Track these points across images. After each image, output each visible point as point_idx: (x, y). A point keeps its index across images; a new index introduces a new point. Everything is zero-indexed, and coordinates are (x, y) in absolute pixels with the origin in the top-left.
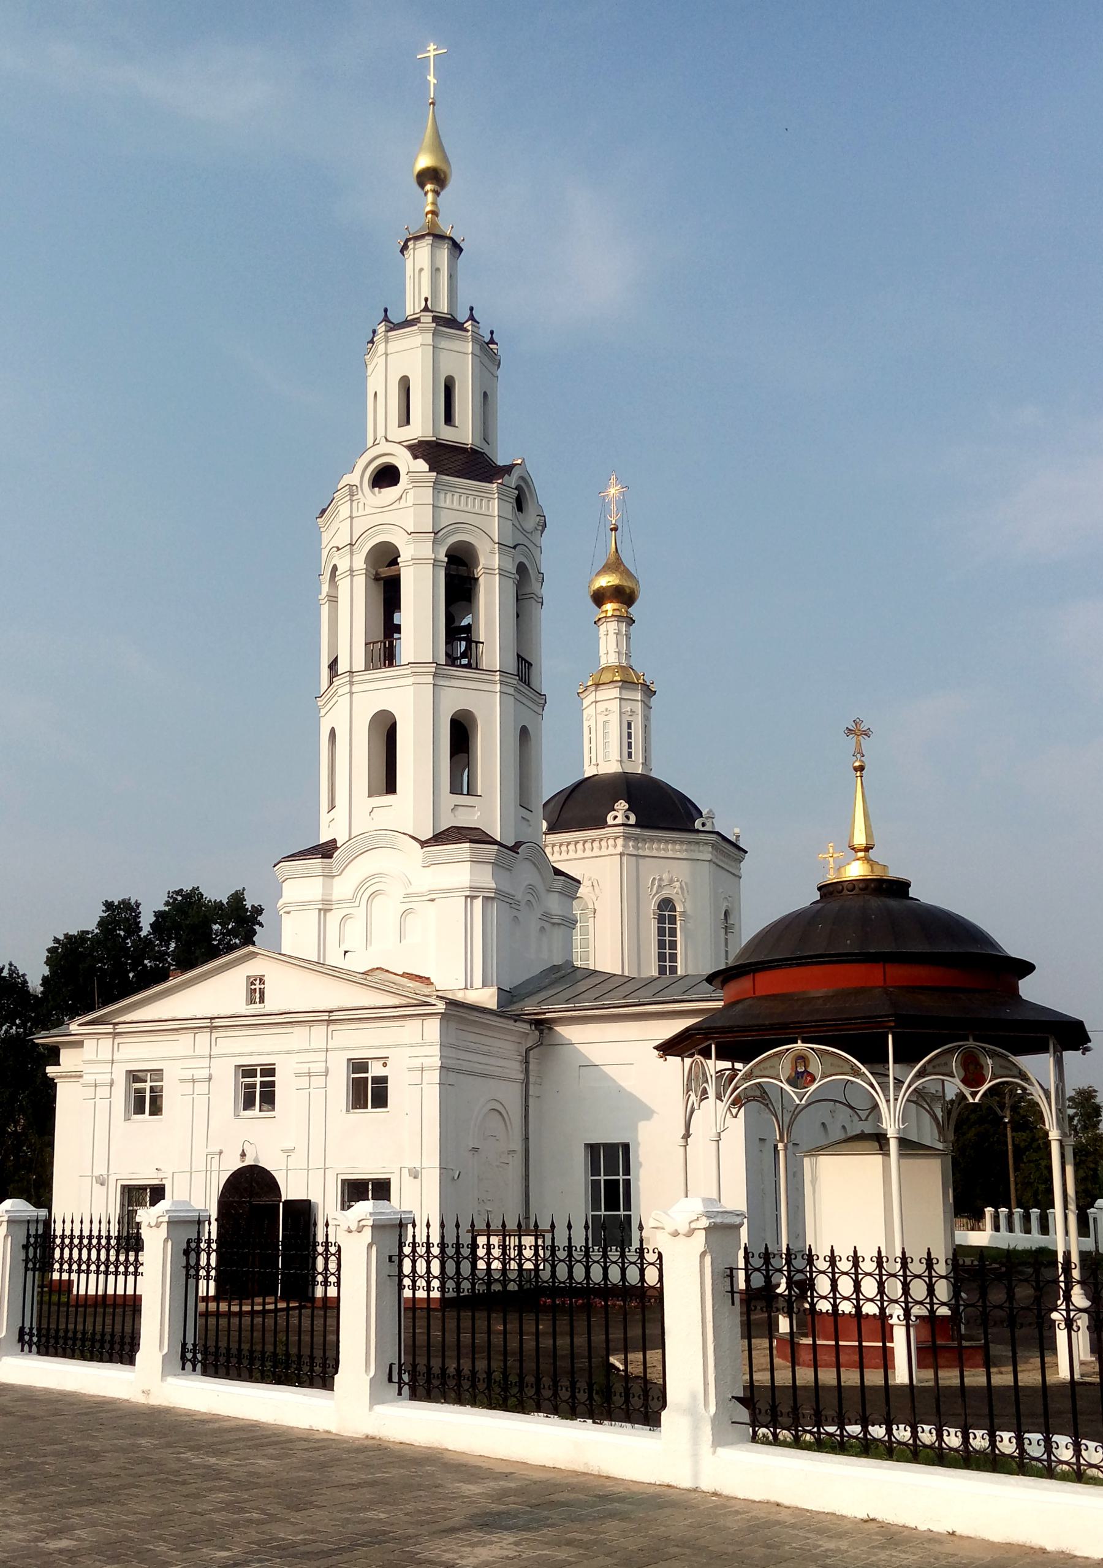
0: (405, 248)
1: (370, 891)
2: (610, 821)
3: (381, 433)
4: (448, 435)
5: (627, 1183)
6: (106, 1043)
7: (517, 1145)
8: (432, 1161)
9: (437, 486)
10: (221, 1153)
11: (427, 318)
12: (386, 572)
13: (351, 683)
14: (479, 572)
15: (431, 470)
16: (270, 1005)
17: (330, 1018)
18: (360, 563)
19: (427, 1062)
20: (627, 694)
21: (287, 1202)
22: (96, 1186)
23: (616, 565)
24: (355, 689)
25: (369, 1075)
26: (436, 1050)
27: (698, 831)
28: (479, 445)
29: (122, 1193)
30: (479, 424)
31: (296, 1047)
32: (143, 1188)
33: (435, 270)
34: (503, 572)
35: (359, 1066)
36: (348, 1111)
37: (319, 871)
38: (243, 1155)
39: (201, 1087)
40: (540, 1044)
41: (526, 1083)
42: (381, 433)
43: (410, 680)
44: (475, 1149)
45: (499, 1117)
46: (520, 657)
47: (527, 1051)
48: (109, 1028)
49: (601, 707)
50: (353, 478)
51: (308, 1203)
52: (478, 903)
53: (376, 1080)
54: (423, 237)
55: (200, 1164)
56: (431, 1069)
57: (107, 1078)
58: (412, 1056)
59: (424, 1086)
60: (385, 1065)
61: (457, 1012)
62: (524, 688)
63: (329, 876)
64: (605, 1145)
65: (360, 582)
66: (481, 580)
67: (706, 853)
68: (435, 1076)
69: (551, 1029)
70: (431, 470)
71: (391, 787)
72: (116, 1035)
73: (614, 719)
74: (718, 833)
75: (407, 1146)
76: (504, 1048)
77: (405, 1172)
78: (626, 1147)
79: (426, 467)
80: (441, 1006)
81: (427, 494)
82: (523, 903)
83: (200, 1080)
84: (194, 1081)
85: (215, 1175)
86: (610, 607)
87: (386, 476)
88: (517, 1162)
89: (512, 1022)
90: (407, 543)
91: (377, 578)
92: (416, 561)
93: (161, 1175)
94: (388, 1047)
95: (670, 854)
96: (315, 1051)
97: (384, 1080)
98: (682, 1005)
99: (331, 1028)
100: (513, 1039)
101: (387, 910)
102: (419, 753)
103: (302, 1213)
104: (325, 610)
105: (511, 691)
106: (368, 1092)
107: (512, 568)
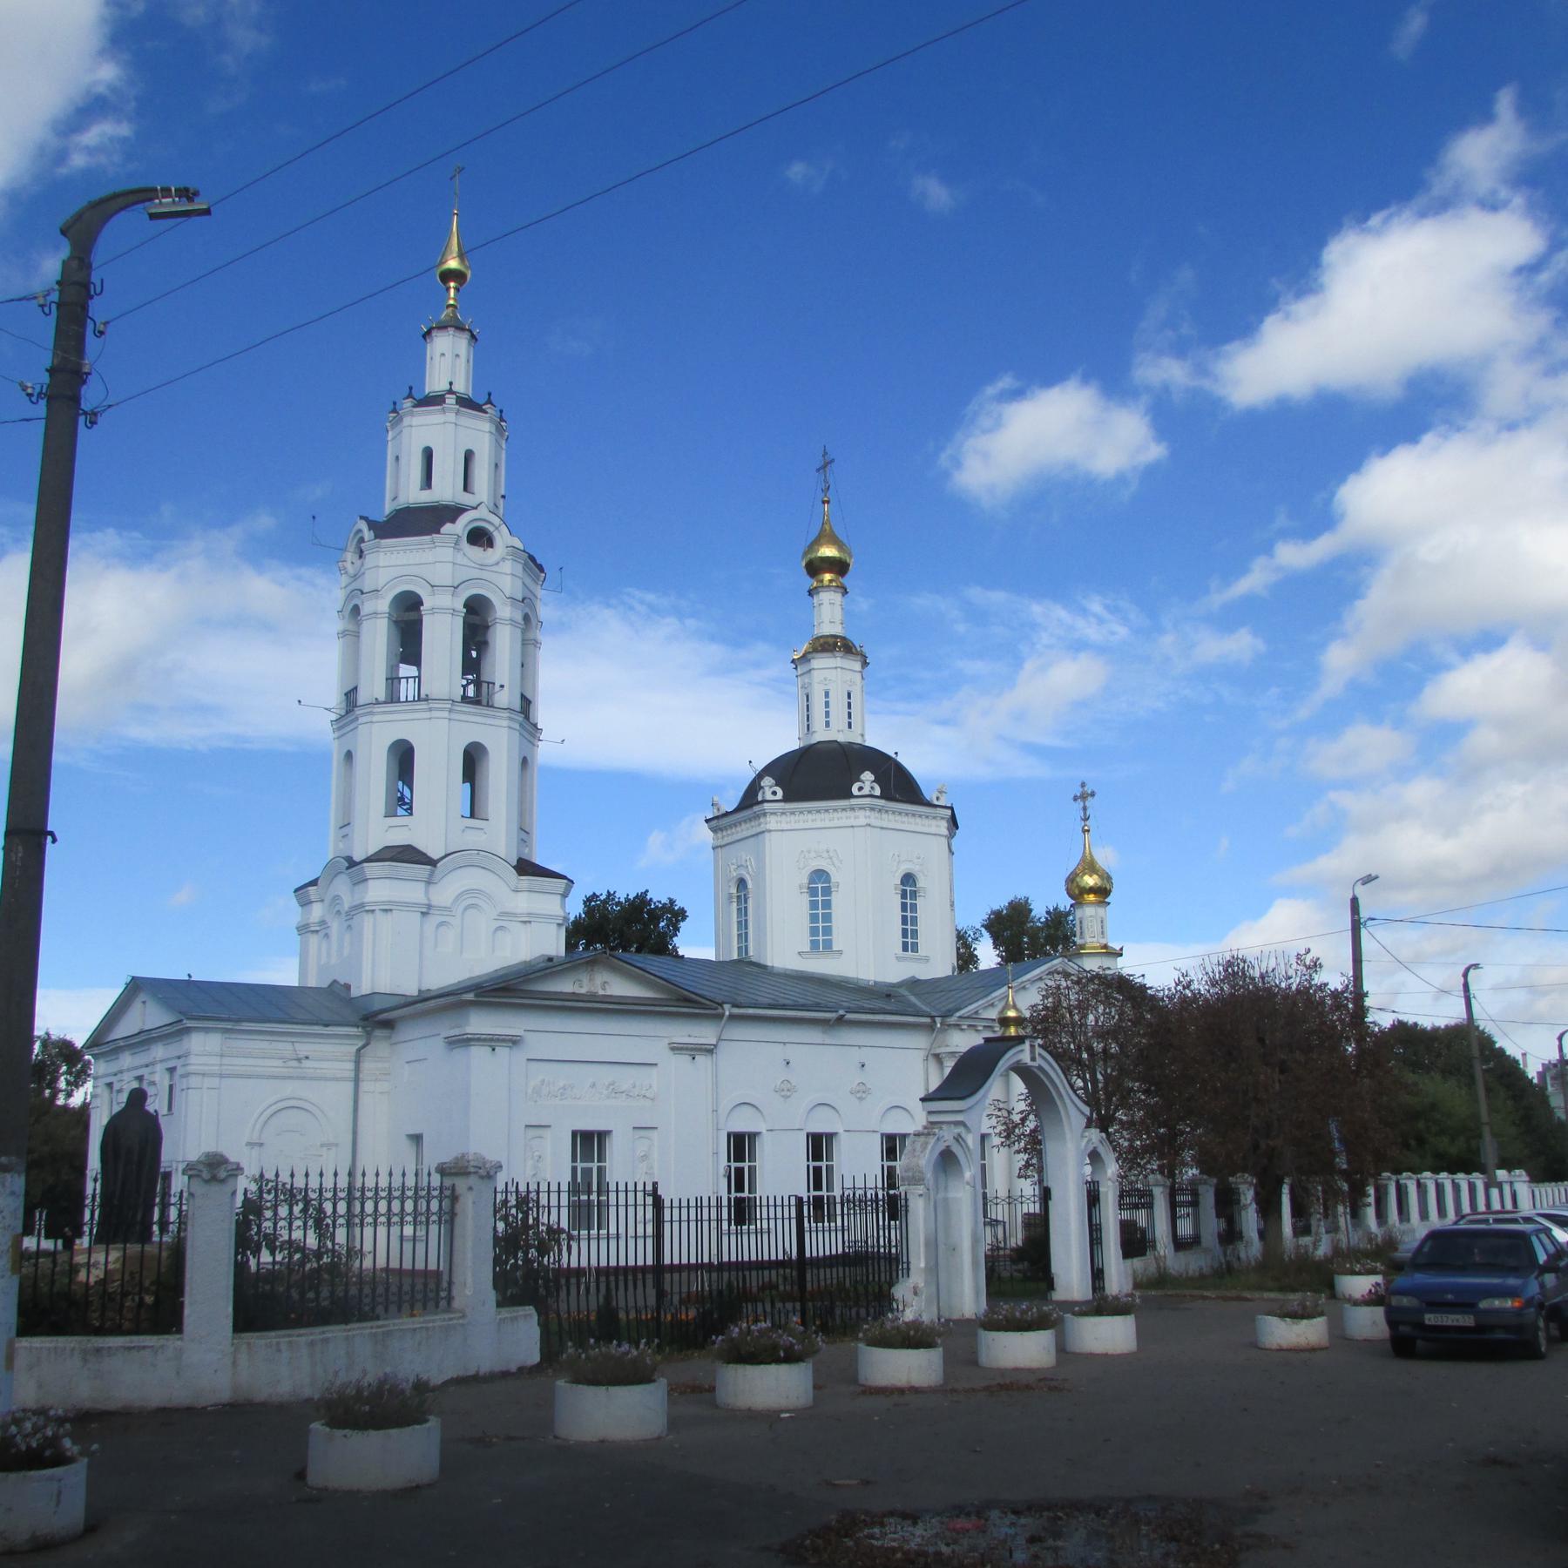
5: (574, 1159)
11: (451, 400)
41: (357, 1081)
45: (290, 1112)
46: (523, 697)
47: (359, 1050)
96: (210, 1055)
107: (519, 617)
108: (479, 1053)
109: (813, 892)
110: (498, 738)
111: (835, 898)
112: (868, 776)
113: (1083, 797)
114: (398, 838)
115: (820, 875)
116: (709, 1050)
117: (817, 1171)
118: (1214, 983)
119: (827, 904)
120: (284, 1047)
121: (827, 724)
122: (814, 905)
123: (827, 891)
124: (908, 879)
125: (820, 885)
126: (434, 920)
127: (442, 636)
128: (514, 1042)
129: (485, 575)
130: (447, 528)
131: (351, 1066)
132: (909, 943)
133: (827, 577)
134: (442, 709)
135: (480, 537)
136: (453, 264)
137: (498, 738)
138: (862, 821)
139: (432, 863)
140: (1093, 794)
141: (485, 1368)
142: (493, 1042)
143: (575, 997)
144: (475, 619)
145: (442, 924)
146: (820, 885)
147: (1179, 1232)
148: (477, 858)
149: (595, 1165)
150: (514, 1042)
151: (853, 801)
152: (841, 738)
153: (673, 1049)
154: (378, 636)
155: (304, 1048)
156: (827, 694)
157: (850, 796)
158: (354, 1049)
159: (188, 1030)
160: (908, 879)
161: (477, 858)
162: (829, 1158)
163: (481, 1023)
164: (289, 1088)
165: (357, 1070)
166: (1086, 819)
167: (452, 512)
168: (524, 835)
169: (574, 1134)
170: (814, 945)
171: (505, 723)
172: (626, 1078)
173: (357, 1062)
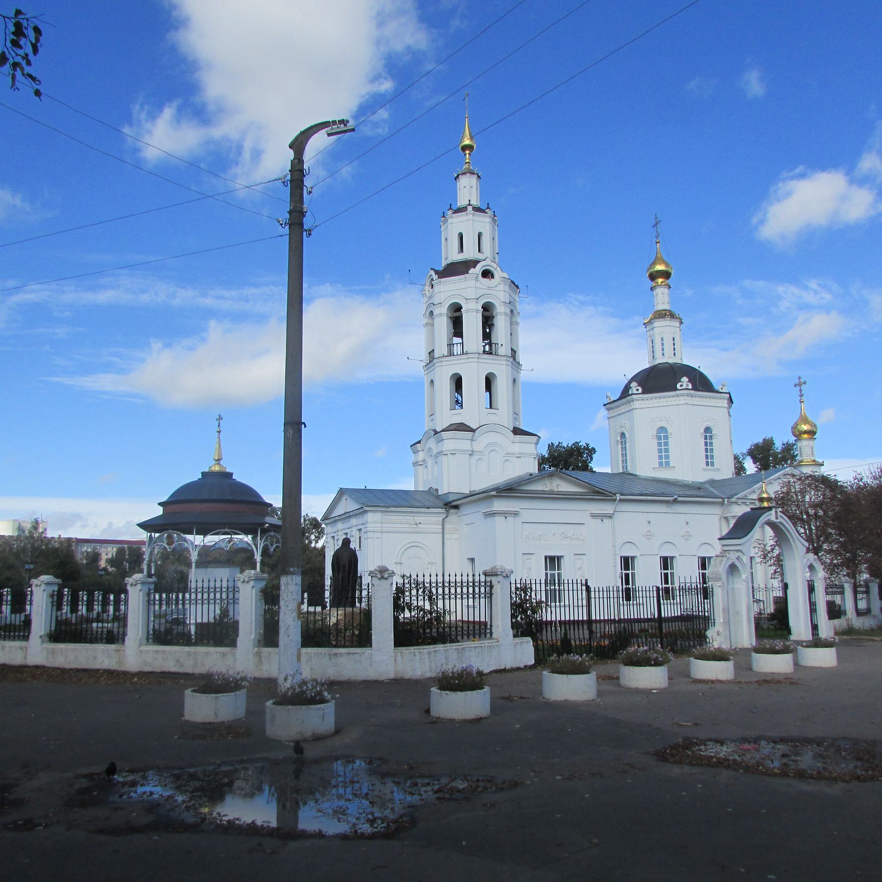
5: (546, 569)
11: (470, 209)
108: (499, 520)
109: (659, 438)
111: (670, 440)
112: (685, 379)
113: (800, 385)
114: (457, 420)
115: (662, 429)
116: (610, 517)
117: (666, 575)
118: (875, 478)
119: (666, 444)
120: (410, 518)
121: (663, 354)
122: (660, 444)
123: (666, 437)
124: (708, 430)
125: (662, 434)
126: (475, 458)
127: (472, 323)
128: (515, 514)
129: (490, 292)
130: (472, 271)
131: (441, 527)
132: (709, 460)
133: (660, 280)
135: (487, 274)
136: (467, 142)
138: (683, 402)
139: (473, 431)
140: (805, 383)
142: (505, 514)
143: (551, 492)
144: (487, 314)
146: (662, 434)
148: (493, 428)
149: (556, 572)
150: (515, 514)
151: (678, 392)
152: (671, 361)
154: (443, 325)
155: (418, 519)
156: (662, 340)
159: (366, 512)
160: (708, 430)
161: (493, 428)
162: (672, 568)
163: (499, 505)
164: (413, 537)
165: (443, 528)
166: (801, 396)
167: (474, 263)
169: (546, 557)
170: (661, 464)
172: (570, 530)
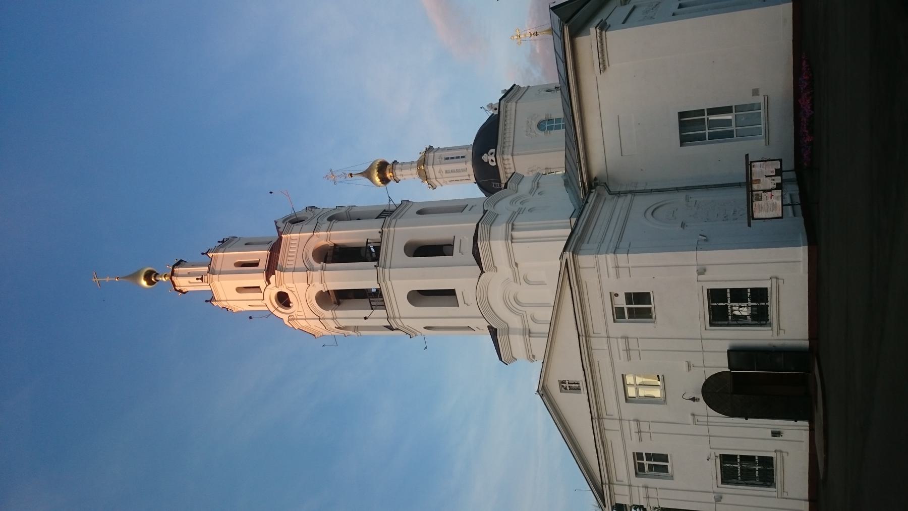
0: (180, 291)
1: (515, 304)
2: (494, 164)
3: (259, 303)
4: (263, 265)
6: (617, 489)
7: (681, 196)
8: (690, 257)
9: (282, 270)
10: (693, 415)
12: (333, 298)
13: (394, 318)
14: (330, 243)
15: (274, 274)
16: (580, 378)
17: (584, 336)
18: (328, 314)
19: (611, 264)
20: (430, 161)
21: (730, 367)
22: (723, 501)
23: (367, 174)
24: (397, 315)
25: (625, 306)
26: (602, 257)
27: (499, 112)
28: (268, 246)
29: (728, 483)
30: (260, 246)
31: (608, 359)
32: (723, 469)
33: (189, 275)
34: (329, 229)
35: (619, 314)
36: (655, 322)
37: (505, 337)
38: (694, 399)
39: (644, 427)
40: (606, 185)
41: (634, 193)
42: (259, 303)
43: (389, 283)
44: (683, 225)
47: (610, 193)
48: (606, 489)
49: (438, 175)
50: (285, 318)
51: (729, 351)
52: (516, 234)
53: (629, 301)
54: (173, 282)
55: (704, 430)
56: (616, 260)
57: (642, 490)
58: (608, 275)
59: (630, 265)
60: (617, 295)
61: (574, 245)
62: (394, 214)
63: (508, 331)
64: (681, 131)
65: (339, 313)
66: (336, 242)
67: (512, 106)
68: (622, 257)
69: (596, 179)
70: (274, 274)
71: (451, 293)
72: (610, 483)
73: (444, 167)
74: (500, 100)
75: (680, 278)
76: (609, 211)
77: (701, 277)
78: (682, 115)
79: (273, 276)
80: (568, 255)
81: (287, 275)
82: (521, 206)
83: (639, 427)
84: (640, 432)
85: (710, 419)
86: (389, 175)
87: (283, 299)
88: (696, 196)
89: (588, 205)
90: (314, 286)
91: (339, 303)
92: (322, 281)
93: (713, 457)
94: (602, 293)
95: (512, 126)
97: (628, 295)
98: (571, 82)
99: (592, 334)
100: (601, 205)
101: (526, 294)
102: (432, 275)
103: (739, 355)
104: (363, 333)
105: (394, 221)
106: (638, 306)
110: (403, 232)
112: (485, 158)
134: (384, 273)
137: (403, 232)
141: (745, 197)
145: (534, 319)
147: (592, 266)
151: (499, 165)
153: (605, 69)
157: (497, 166)
158: (610, 197)
168: (467, 208)
171: (392, 229)
173: (619, 194)
